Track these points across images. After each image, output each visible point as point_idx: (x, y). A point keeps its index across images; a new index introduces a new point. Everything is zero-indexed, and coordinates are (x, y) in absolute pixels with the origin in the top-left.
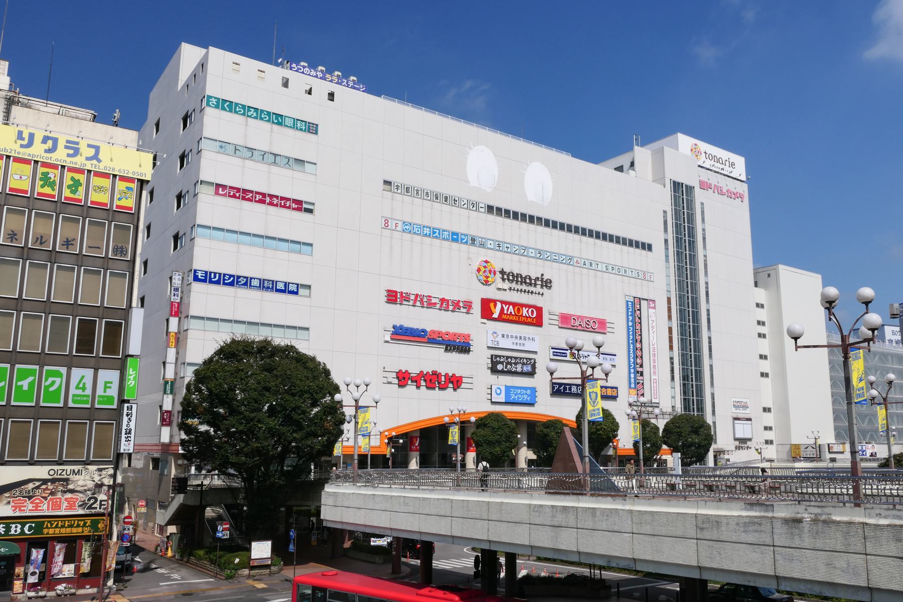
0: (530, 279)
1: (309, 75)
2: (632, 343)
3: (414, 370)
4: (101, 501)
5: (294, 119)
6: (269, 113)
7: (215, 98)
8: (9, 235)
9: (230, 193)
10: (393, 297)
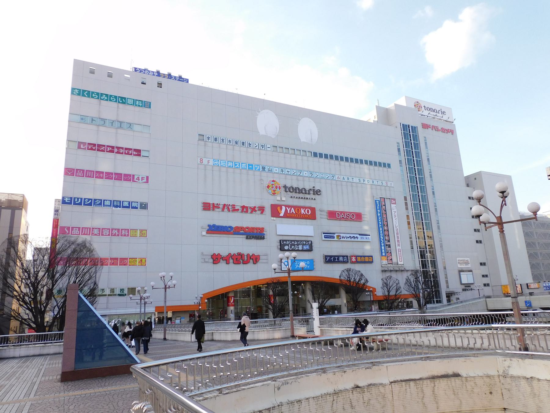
3: (224, 253)
5: (134, 100)
6: (116, 97)
10: (207, 207)
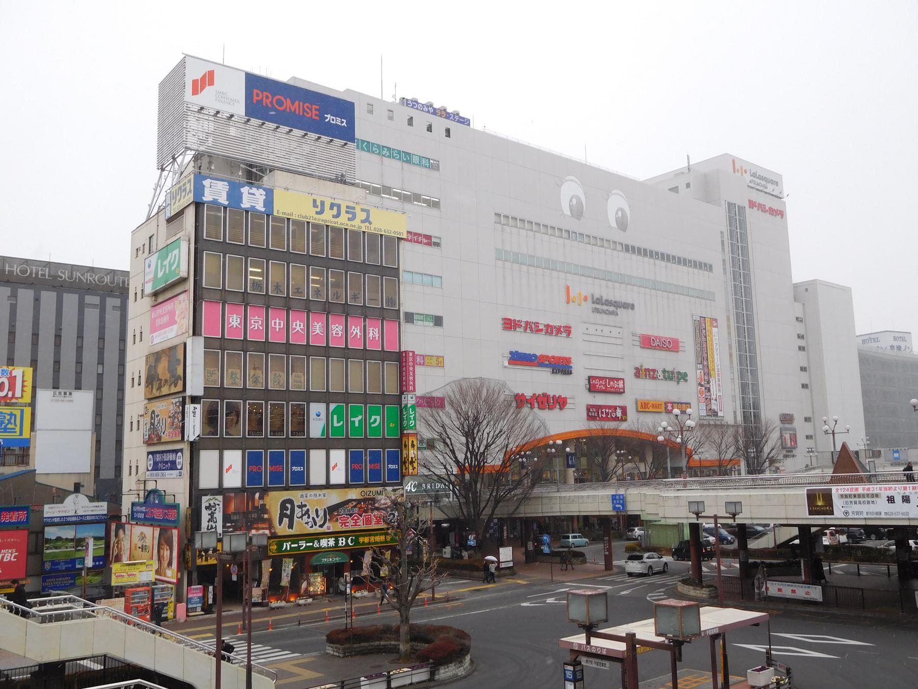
1: (423, 110)
3: (528, 394)
5: (420, 157)
6: (399, 152)
8: (315, 291)
10: (510, 325)
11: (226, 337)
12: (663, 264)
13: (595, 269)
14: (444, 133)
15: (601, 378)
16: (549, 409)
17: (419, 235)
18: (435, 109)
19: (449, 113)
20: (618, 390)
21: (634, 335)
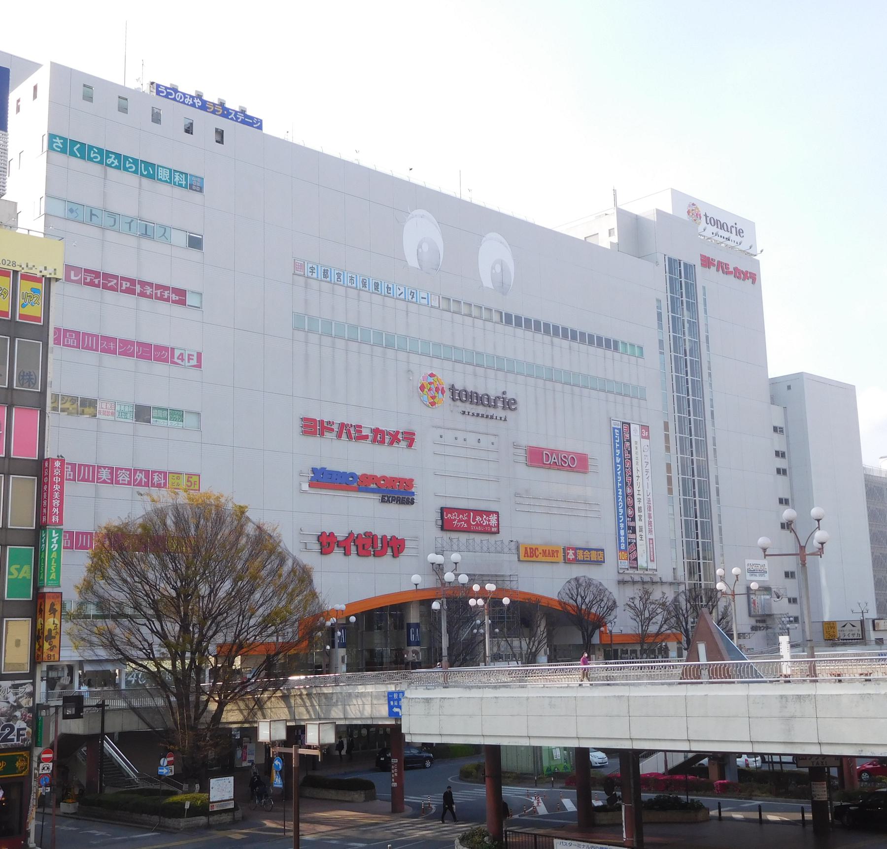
0: (488, 399)
1: (183, 102)
2: (621, 487)
3: (341, 534)
4: (19, 730)
6: (135, 161)
7: (61, 138)
9: (85, 279)
11: (12, 456)
12: (565, 343)
13: (455, 348)
14: (213, 136)
15: (461, 511)
16: (374, 555)
17: (166, 288)
18: (204, 102)
19: (227, 109)
20: (488, 529)
21: (516, 446)
